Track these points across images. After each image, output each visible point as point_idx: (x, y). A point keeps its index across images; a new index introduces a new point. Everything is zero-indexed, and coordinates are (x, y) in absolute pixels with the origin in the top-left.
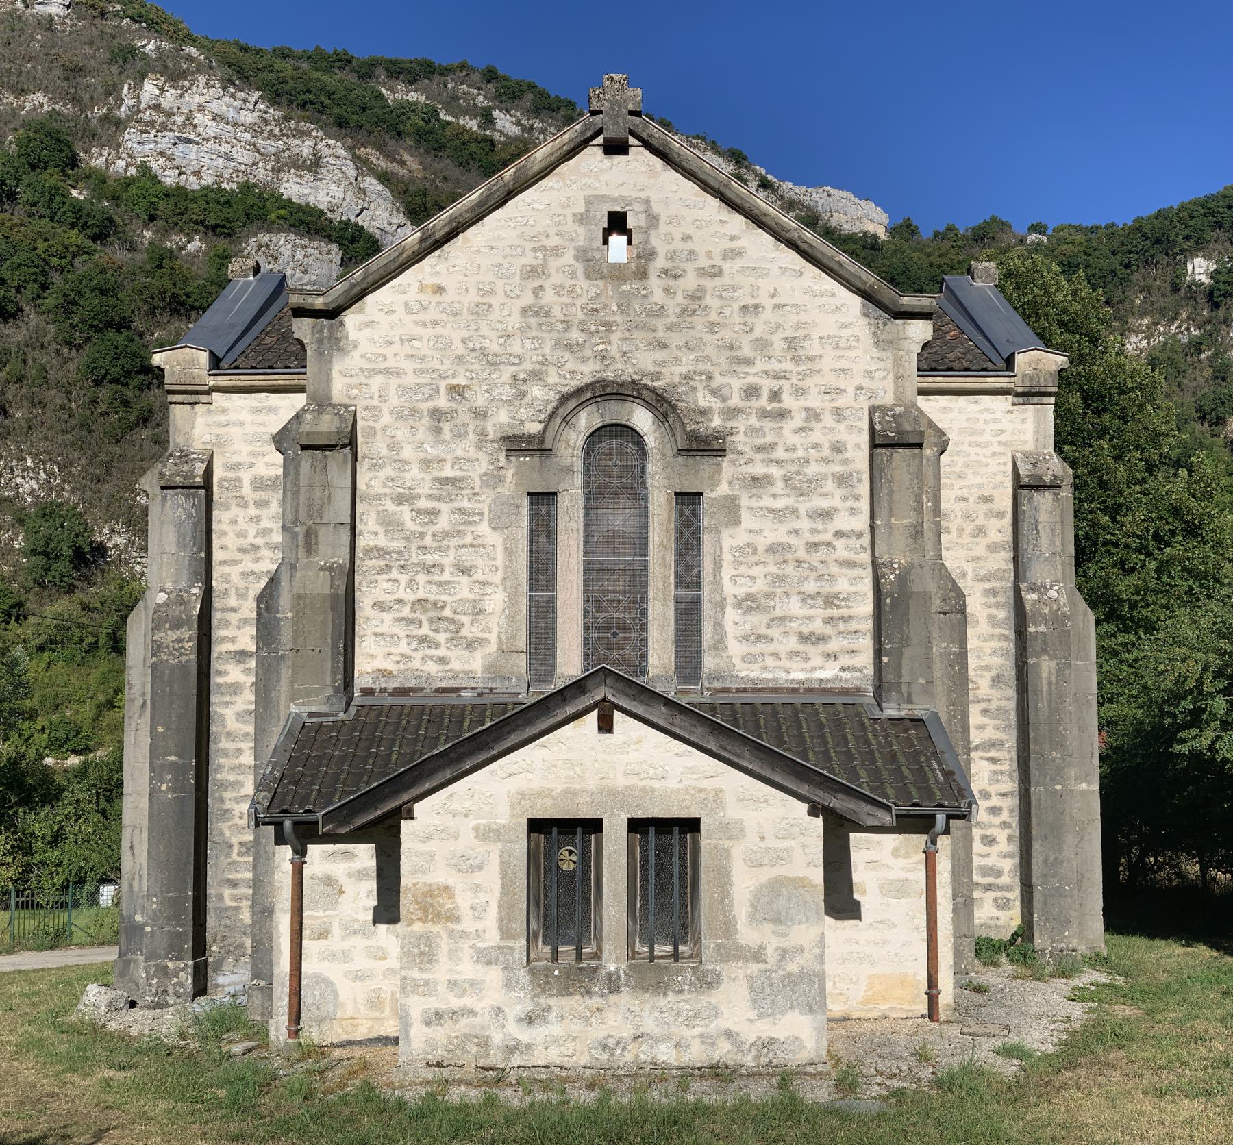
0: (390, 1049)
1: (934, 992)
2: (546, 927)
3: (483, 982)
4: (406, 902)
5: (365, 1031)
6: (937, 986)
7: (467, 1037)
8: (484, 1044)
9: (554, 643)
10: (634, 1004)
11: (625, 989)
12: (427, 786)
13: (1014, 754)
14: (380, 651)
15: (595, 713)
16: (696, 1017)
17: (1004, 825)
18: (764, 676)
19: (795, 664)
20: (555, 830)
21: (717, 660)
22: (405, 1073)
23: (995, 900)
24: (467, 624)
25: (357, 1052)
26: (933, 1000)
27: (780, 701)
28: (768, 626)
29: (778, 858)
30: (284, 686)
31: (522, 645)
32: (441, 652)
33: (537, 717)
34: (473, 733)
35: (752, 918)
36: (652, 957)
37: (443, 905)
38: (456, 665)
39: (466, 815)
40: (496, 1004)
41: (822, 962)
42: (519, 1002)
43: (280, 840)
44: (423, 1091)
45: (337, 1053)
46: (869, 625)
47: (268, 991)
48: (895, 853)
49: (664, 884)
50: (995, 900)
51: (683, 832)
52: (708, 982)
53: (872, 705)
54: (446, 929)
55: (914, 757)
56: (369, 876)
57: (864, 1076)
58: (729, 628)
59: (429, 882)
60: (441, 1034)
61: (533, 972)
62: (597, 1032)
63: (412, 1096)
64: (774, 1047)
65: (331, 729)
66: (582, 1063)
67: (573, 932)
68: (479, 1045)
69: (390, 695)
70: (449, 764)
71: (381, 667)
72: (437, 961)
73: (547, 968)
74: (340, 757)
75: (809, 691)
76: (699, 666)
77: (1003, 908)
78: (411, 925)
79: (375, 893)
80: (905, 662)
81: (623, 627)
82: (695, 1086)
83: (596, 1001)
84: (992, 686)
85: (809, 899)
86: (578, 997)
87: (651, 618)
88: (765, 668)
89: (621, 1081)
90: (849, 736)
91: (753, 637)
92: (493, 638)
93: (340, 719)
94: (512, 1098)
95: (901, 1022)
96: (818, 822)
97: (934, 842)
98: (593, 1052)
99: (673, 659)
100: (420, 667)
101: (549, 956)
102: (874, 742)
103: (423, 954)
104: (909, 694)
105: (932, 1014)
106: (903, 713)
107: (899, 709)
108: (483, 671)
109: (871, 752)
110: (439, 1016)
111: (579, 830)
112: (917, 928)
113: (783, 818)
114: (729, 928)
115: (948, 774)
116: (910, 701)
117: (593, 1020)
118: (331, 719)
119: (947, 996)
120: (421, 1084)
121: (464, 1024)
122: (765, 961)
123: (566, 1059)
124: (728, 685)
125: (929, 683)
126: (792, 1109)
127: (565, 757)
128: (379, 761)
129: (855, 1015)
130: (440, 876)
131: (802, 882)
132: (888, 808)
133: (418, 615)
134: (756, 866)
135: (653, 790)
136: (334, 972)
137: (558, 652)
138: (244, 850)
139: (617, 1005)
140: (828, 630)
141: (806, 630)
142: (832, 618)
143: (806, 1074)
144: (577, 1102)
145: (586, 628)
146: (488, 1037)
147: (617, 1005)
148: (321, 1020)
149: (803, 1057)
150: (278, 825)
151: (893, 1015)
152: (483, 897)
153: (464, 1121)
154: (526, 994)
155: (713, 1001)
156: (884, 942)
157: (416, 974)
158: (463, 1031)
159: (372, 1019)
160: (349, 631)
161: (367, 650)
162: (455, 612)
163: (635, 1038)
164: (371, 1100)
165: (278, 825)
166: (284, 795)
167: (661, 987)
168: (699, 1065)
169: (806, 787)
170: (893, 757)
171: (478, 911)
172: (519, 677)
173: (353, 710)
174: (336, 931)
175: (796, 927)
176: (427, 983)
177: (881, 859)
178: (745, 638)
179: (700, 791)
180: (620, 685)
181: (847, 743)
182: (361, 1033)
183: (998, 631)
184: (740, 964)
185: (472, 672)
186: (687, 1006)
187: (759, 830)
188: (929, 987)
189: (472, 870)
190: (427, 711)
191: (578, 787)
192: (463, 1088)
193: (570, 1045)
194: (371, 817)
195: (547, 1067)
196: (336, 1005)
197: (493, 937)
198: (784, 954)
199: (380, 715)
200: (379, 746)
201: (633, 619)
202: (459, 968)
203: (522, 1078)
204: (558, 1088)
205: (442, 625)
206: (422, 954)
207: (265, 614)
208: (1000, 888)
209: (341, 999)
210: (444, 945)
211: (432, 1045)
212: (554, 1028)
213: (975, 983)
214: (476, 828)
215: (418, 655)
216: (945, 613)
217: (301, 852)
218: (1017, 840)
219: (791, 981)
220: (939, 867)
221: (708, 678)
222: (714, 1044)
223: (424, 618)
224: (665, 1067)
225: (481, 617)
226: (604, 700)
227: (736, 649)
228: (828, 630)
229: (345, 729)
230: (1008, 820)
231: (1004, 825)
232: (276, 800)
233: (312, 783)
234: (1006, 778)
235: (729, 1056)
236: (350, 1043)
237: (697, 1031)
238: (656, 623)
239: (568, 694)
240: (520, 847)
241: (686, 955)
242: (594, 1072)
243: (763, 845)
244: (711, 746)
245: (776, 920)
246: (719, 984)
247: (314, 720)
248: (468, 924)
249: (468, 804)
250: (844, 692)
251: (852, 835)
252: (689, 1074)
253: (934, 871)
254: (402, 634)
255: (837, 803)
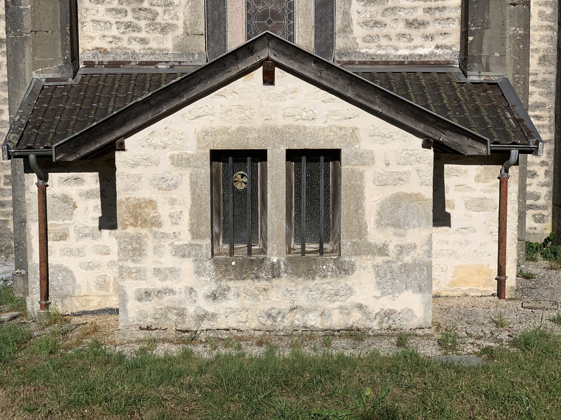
0: (113, 317)
1: (503, 278)
2: (225, 230)
3: (179, 270)
4: (121, 212)
5: (96, 304)
6: (505, 274)
7: (169, 309)
8: (181, 313)
9: (225, 28)
10: (291, 286)
11: (284, 275)
12: (134, 125)
13: (553, 113)
14: (97, 34)
15: (261, 69)
16: (336, 294)
17: (543, 163)
18: (379, 52)
19: (402, 44)
20: (230, 159)
21: (345, 40)
22: (124, 335)
23: (534, 216)
24: (161, 14)
25: (90, 319)
26: (501, 284)
27: (391, 71)
28: (383, 15)
29: (399, 180)
30: (28, 60)
31: (202, 30)
32: (143, 35)
33: (217, 73)
34: (165, 91)
35: (379, 224)
36: (303, 252)
37: (148, 214)
38: (153, 45)
39: (164, 148)
40: (190, 285)
41: (430, 256)
42: (207, 284)
43: (28, 169)
44: (137, 347)
45: (76, 320)
46: (457, 14)
47: (25, 277)
48: (477, 179)
49: (313, 199)
50: (534, 216)
51: (327, 161)
52: (345, 270)
53: (459, 73)
54: (151, 231)
55: (493, 109)
56: (95, 195)
57: (459, 338)
58: (354, 16)
59: (137, 197)
60: (149, 306)
61: (216, 263)
62: (264, 305)
63: (129, 351)
64: (393, 316)
65: (63, 90)
66: (253, 327)
67: (244, 234)
68: (177, 315)
69: (106, 66)
70: (151, 109)
71: (98, 46)
72: (145, 255)
73: (226, 260)
74: (70, 110)
75: (412, 63)
76: (332, 45)
77: (539, 222)
78: (127, 229)
79: (100, 207)
80: (485, 41)
81: (276, 16)
82: (336, 342)
83: (263, 284)
84: (539, 64)
85: (421, 210)
86: (249, 281)
87: (296, 8)
88: (380, 47)
89: (281, 340)
90: (443, 95)
91: (371, 23)
92: (180, 23)
93: (69, 83)
94: (202, 352)
95: (479, 299)
96: (430, 153)
97: (506, 171)
98: (261, 319)
99: (313, 40)
100: (127, 46)
101: (228, 251)
102: (462, 99)
103: (134, 249)
104: (487, 64)
105: (500, 293)
106: (482, 79)
107: (479, 76)
108: (174, 49)
109: (460, 106)
110: (148, 294)
111: (249, 159)
112: (491, 233)
113: (404, 150)
114: (361, 231)
115: (519, 121)
116: (488, 70)
117: (261, 297)
118: (63, 83)
119: (511, 280)
120: (136, 342)
121: (167, 299)
122: (387, 255)
123: (241, 324)
124: (353, 59)
125: (503, 56)
126: (418, 364)
127: (238, 103)
128: (99, 112)
129: (444, 294)
130: (146, 192)
131: (416, 197)
132: (484, 142)
133: (124, 6)
134: (382, 185)
135: (305, 128)
136: (71, 263)
137: (229, 35)
138: (8, 181)
139: (278, 287)
140: (427, 17)
141: (411, 18)
142: (430, 9)
143: (416, 335)
144: (251, 355)
145: (249, 17)
146: (184, 309)
147: (278, 287)
148: (64, 297)
149: (414, 323)
150: (26, 158)
151: (472, 294)
152: (178, 208)
153: (169, 372)
154: (211, 279)
155: (349, 283)
156: (467, 242)
157: (130, 264)
158: (166, 305)
159: (101, 296)
160: (74, 18)
161: (88, 33)
162: (151, 4)
163: (292, 310)
164: (100, 355)
165: (26, 158)
166: (29, 136)
167: (310, 274)
168: (338, 328)
169: (422, 126)
170: (477, 110)
171: (175, 218)
172: (200, 54)
173: (79, 77)
174: (72, 235)
175: (411, 230)
176: (138, 271)
177: (470, 184)
178: (365, 23)
179: (341, 129)
180: (280, 48)
181: (442, 100)
182: (93, 306)
183: (546, 23)
184: (369, 257)
185: (165, 49)
186: (329, 287)
187: (385, 158)
188: (498, 275)
189: (169, 188)
190: (134, 78)
191: (248, 126)
192: (166, 345)
193: (244, 314)
194: (92, 148)
195: (228, 330)
196: (74, 287)
197: (186, 238)
198: (402, 250)
199: (99, 80)
200: (98, 102)
201: (283, 10)
202: (162, 260)
203: (209, 338)
204: (236, 344)
205: (142, 14)
206: (134, 249)
207: (11, 6)
208: (537, 207)
209: (77, 282)
210: (150, 243)
211: (143, 314)
212: (232, 303)
213: (524, 272)
214: (172, 157)
215: (125, 37)
216: (514, 5)
217: (43, 178)
218: (552, 174)
219: (407, 269)
220: (510, 189)
221: (338, 54)
222: (348, 314)
223: (129, 9)
224: (313, 330)
225: (171, 8)
226: (268, 59)
227: (358, 32)
228: (427, 17)
229: (73, 90)
230: (546, 160)
231: (543, 163)
232: (23, 140)
233: (50, 127)
234: (546, 130)
235: (360, 322)
236: (85, 313)
237: (337, 304)
238: (301, 12)
239: (240, 55)
240: (205, 171)
241: (328, 250)
242: (261, 333)
243: (388, 169)
244: (349, 94)
245: (397, 225)
246: (353, 271)
247: (51, 84)
248: (167, 228)
249: (165, 139)
250: (438, 64)
251: (446, 166)
252: (330, 335)
253: (506, 192)
254: (113, 21)
255: (444, 138)
